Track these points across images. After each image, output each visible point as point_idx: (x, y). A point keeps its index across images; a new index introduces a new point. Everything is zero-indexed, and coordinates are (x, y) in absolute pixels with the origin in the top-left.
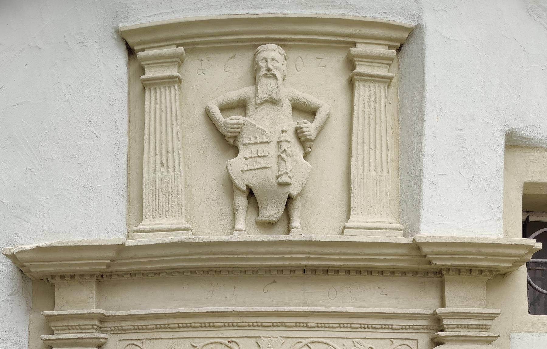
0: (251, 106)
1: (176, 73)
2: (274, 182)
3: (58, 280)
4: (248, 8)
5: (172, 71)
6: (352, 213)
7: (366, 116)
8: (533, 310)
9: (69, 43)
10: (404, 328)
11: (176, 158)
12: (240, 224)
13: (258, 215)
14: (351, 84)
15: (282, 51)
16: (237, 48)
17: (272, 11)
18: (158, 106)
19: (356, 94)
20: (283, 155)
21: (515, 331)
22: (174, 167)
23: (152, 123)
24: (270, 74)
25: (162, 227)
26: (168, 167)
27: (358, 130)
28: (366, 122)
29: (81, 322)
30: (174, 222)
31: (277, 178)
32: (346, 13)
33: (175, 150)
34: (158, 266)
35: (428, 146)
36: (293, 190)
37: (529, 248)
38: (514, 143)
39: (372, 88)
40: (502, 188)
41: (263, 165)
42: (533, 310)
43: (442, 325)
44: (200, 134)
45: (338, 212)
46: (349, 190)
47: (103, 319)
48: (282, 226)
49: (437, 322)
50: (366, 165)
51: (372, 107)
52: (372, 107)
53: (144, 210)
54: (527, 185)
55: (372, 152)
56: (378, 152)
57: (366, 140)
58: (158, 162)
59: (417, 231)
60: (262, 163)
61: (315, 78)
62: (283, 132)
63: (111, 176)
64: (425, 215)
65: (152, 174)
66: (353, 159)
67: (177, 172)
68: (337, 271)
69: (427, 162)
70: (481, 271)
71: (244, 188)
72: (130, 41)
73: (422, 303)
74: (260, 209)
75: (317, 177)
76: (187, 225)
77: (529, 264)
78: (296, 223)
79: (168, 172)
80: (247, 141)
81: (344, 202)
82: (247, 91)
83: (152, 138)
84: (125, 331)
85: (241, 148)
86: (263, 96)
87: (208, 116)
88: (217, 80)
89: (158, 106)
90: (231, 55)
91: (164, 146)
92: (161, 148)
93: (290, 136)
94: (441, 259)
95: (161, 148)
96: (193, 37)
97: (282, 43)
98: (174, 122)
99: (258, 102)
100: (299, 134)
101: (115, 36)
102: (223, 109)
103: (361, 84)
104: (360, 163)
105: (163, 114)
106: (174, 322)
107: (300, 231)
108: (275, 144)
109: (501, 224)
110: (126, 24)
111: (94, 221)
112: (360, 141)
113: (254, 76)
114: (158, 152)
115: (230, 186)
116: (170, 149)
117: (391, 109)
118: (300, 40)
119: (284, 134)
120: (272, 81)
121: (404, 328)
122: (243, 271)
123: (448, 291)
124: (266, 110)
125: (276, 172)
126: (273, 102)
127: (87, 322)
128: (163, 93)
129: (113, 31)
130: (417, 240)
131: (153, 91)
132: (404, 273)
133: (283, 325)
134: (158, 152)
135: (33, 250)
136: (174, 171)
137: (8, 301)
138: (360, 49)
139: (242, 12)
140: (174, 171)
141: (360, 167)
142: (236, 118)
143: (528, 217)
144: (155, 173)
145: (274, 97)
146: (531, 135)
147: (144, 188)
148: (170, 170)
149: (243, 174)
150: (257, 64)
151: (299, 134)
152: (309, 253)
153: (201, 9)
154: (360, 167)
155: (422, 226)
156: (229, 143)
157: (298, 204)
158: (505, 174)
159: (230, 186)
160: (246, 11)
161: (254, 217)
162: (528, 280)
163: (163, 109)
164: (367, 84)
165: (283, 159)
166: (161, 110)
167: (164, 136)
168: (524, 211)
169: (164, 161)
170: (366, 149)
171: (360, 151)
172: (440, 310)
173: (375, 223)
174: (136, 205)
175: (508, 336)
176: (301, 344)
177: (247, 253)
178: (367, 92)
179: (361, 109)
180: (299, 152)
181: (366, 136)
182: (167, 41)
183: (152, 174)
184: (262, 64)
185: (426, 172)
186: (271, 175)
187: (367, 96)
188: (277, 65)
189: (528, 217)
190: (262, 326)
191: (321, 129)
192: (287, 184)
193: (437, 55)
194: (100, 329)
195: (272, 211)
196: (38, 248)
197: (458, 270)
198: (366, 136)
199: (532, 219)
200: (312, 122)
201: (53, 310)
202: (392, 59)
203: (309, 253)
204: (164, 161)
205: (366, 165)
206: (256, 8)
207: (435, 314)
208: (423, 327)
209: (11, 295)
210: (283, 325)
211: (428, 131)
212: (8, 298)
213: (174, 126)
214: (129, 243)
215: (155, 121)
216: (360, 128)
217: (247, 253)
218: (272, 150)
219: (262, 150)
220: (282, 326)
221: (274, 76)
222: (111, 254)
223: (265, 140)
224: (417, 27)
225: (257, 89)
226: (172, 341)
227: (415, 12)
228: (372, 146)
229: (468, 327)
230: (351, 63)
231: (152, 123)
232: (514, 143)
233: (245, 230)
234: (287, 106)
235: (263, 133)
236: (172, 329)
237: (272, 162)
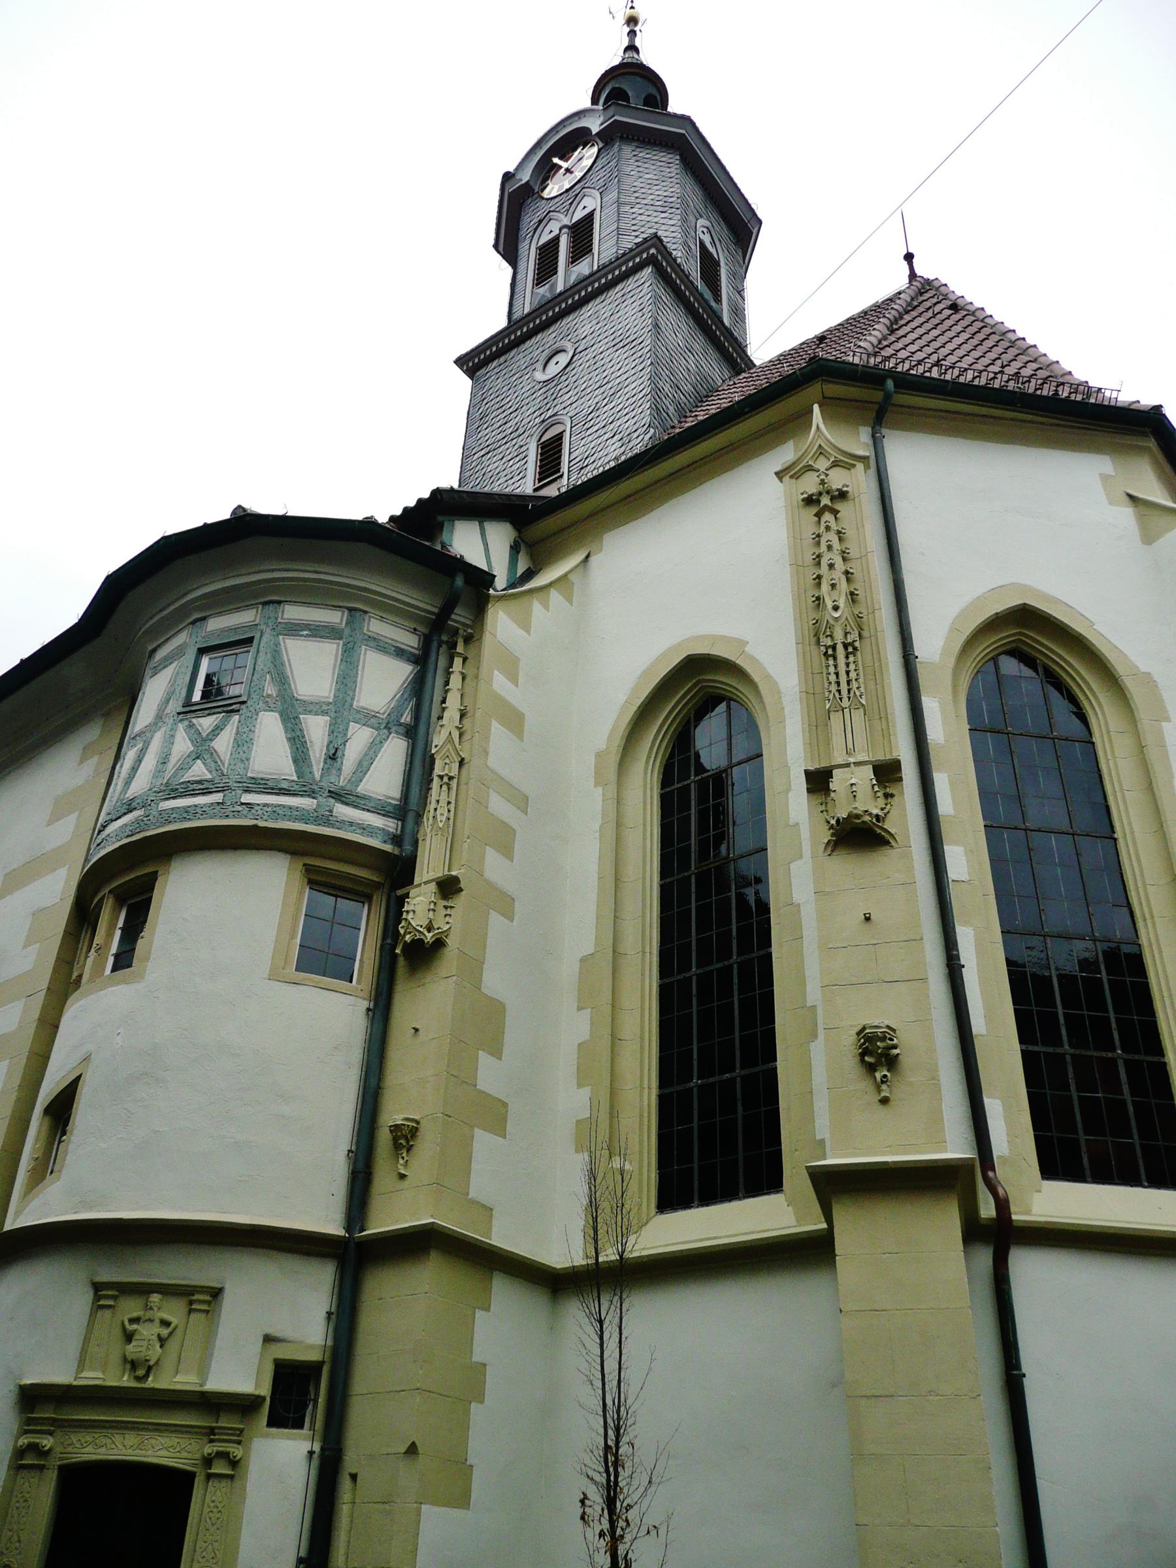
5: (111, 1303)
12: (125, 1378)
24: (151, 1309)
25: (92, 1377)
35: (218, 1343)
38: (268, 1339)
44: (117, 1332)
47: (55, 1420)
61: (173, 1310)
63: (73, 1348)
88: (130, 1307)
93: (155, 1338)
107: (151, 1383)
111: (60, 1374)
115: (125, 1359)
126: (151, 1320)
142: (135, 1326)
173: (185, 1381)
174: (81, 1365)
180: (158, 1345)
191: (171, 1334)
193: (228, 1299)
214: (75, 1383)
219: (141, 1343)
230: (191, 1303)
233: (126, 1381)
234: (157, 1322)
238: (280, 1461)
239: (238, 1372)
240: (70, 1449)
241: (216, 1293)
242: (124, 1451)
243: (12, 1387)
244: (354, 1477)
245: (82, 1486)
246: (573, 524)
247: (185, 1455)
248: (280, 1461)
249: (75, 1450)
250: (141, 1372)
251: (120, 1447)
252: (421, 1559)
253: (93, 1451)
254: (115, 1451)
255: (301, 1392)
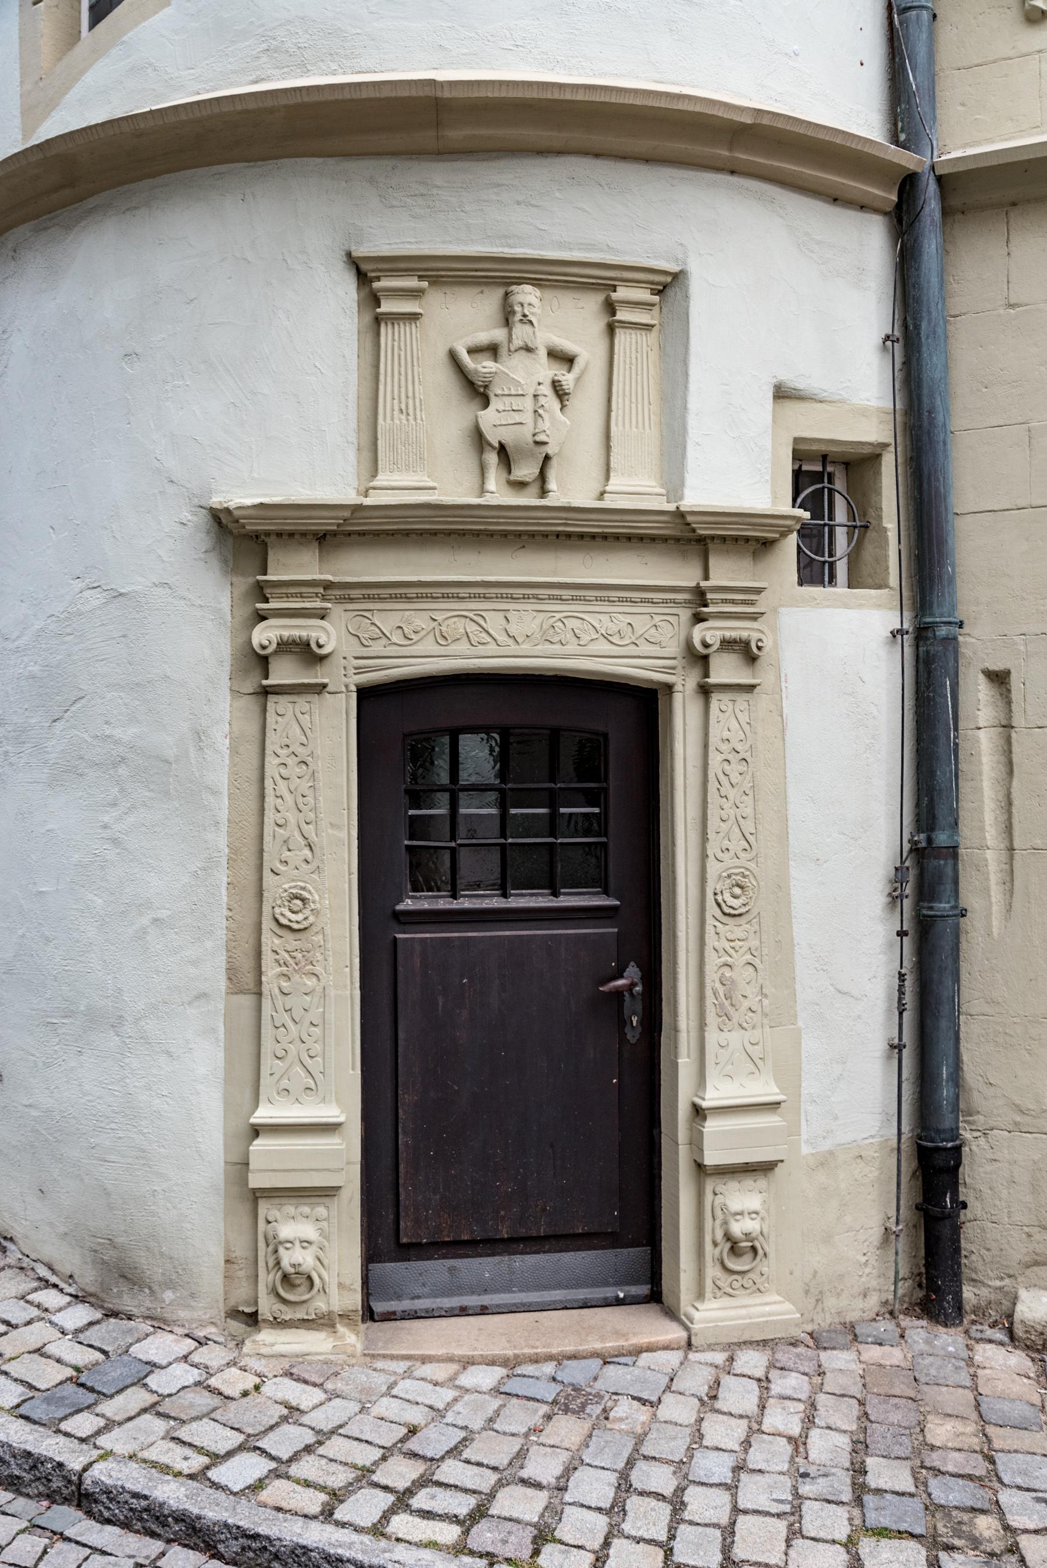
0: (503, 351)
1: (418, 310)
2: (530, 440)
3: (273, 537)
4: (503, 246)
6: (612, 474)
7: (627, 367)
8: (801, 583)
9: (289, 262)
10: (665, 602)
11: (418, 404)
12: (491, 484)
13: (510, 472)
14: (611, 329)
15: (538, 292)
16: (487, 284)
17: (528, 251)
18: (396, 344)
19: (616, 342)
20: (541, 411)
21: (783, 606)
22: (415, 415)
23: (389, 362)
24: (526, 320)
25: (401, 485)
26: (408, 414)
27: (618, 382)
28: (628, 373)
29: (304, 590)
30: (416, 478)
31: (534, 435)
32: (608, 257)
33: (417, 395)
34: (395, 527)
35: (693, 403)
36: (550, 450)
37: (797, 519)
38: (782, 394)
39: (633, 336)
40: (770, 447)
41: (518, 421)
42: (801, 583)
43: (706, 600)
44: (443, 378)
45: (596, 472)
46: (608, 448)
47: (328, 586)
48: (534, 489)
49: (700, 596)
50: (627, 421)
51: (634, 356)
52: (634, 356)
53: (380, 462)
54: (796, 440)
55: (633, 406)
56: (640, 406)
57: (627, 393)
58: (396, 408)
59: (681, 498)
60: (517, 418)
61: (563, 320)
62: (539, 384)
64: (690, 479)
65: (389, 421)
66: (613, 414)
67: (419, 421)
68: (593, 536)
69: (692, 421)
70: (747, 539)
71: (497, 445)
72: (364, 267)
73: (683, 574)
74: (512, 467)
75: (571, 432)
76: (431, 484)
77: (798, 531)
78: (552, 485)
79: (408, 420)
80: (500, 392)
81: (602, 461)
82: (498, 334)
83: (389, 379)
84: (351, 600)
85: (493, 400)
86: (517, 342)
87: (453, 356)
88: (462, 318)
89: (396, 344)
90: (479, 289)
91: (403, 390)
92: (400, 392)
93: (546, 389)
94: (705, 529)
95: (400, 392)
96: (438, 270)
97: (537, 283)
98: (415, 364)
99: (512, 349)
100: (557, 387)
101: (345, 259)
102: (471, 351)
103: (622, 331)
104: (620, 419)
105: (402, 353)
106: (412, 591)
107: (557, 497)
108: (531, 397)
109: (768, 486)
110: (362, 249)
111: (327, 481)
112: (621, 393)
113: (507, 316)
114: (396, 397)
115: (479, 439)
116: (410, 394)
117: (654, 356)
118: (557, 281)
119: (541, 387)
120: (527, 328)
121: (665, 602)
122: (491, 534)
123: (712, 561)
124: (521, 357)
125: (532, 429)
127: (311, 590)
128: (402, 330)
129: (343, 253)
130: (682, 509)
131: (390, 326)
132: (665, 539)
133: (536, 597)
134: (396, 397)
135: (254, 506)
136: (415, 419)
137: (201, 559)
138: (622, 293)
139: (495, 250)
140: (415, 419)
141: (620, 423)
143: (800, 466)
144: (392, 419)
145: (530, 345)
146: (801, 387)
147: (379, 437)
148: (411, 418)
149: (495, 429)
150: (511, 306)
151: (557, 387)
152: (566, 519)
153: (450, 242)
154: (620, 423)
155: (687, 492)
156: (478, 392)
157: (554, 463)
158: (773, 429)
159: (479, 439)
160: (500, 250)
161: (505, 475)
162: (798, 545)
163: (403, 348)
164: (628, 331)
165: (540, 415)
166: (400, 348)
167: (403, 378)
168: (795, 458)
169: (403, 407)
170: (627, 402)
171: (621, 405)
172: (703, 584)
175: (775, 611)
176: (554, 619)
177: (499, 517)
178: (628, 339)
179: (622, 359)
180: (556, 405)
181: (627, 388)
182: (407, 272)
183: (389, 421)
184: (518, 308)
185: (690, 431)
186: (526, 433)
187: (628, 344)
188: (534, 310)
189: (800, 466)
190: (512, 598)
191: (578, 380)
192: (545, 443)
193: (696, 286)
194: (324, 599)
195: (526, 471)
196: (262, 505)
197: (724, 539)
198: (627, 388)
199: (805, 468)
200: (569, 371)
201: (265, 574)
202: (653, 305)
203: (566, 519)
204: (403, 407)
205: (627, 421)
206: (511, 247)
207: (698, 587)
208: (686, 601)
209: (206, 552)
210: (536, 597)
211: (693, 387)
212: (202, 556)
213: (416, 368)
214: (368, 501)
215: (393, 360)
216: (621, 379)
217: (499, 517)
218: (528, 404)
219: (517, 404)
220: (534, 598)
221: (531, 322)
222: (347, 514)
223: (521, 392)
224: (681, 272)
225: (510, 335)
226: (407, 613)
227: (680, 256)
228: (634, 400)
229: (733, 602)
230: (610, 308)
231: (389, 362)
232: (782, 394)
233: (497, 493)
234: (543, 353)
235: (518, 384)
236: (407, 599)
237: (528, 418)
238: (834, 651)
239: (740, 475)
240: (377, 648)
241: (668, 285)
242: (514, 649)
243: (186, 515)
244: (999, 679)
245: (406, 728)
246: (614, 1363)
247: (645, 649)
248: (834, 651)
249: (392, 650)
250: (526, 471)
251: (502, 638)
252: (17, 3)
253: (436, 650)
254: (491, 648)
255: (873, 503)
